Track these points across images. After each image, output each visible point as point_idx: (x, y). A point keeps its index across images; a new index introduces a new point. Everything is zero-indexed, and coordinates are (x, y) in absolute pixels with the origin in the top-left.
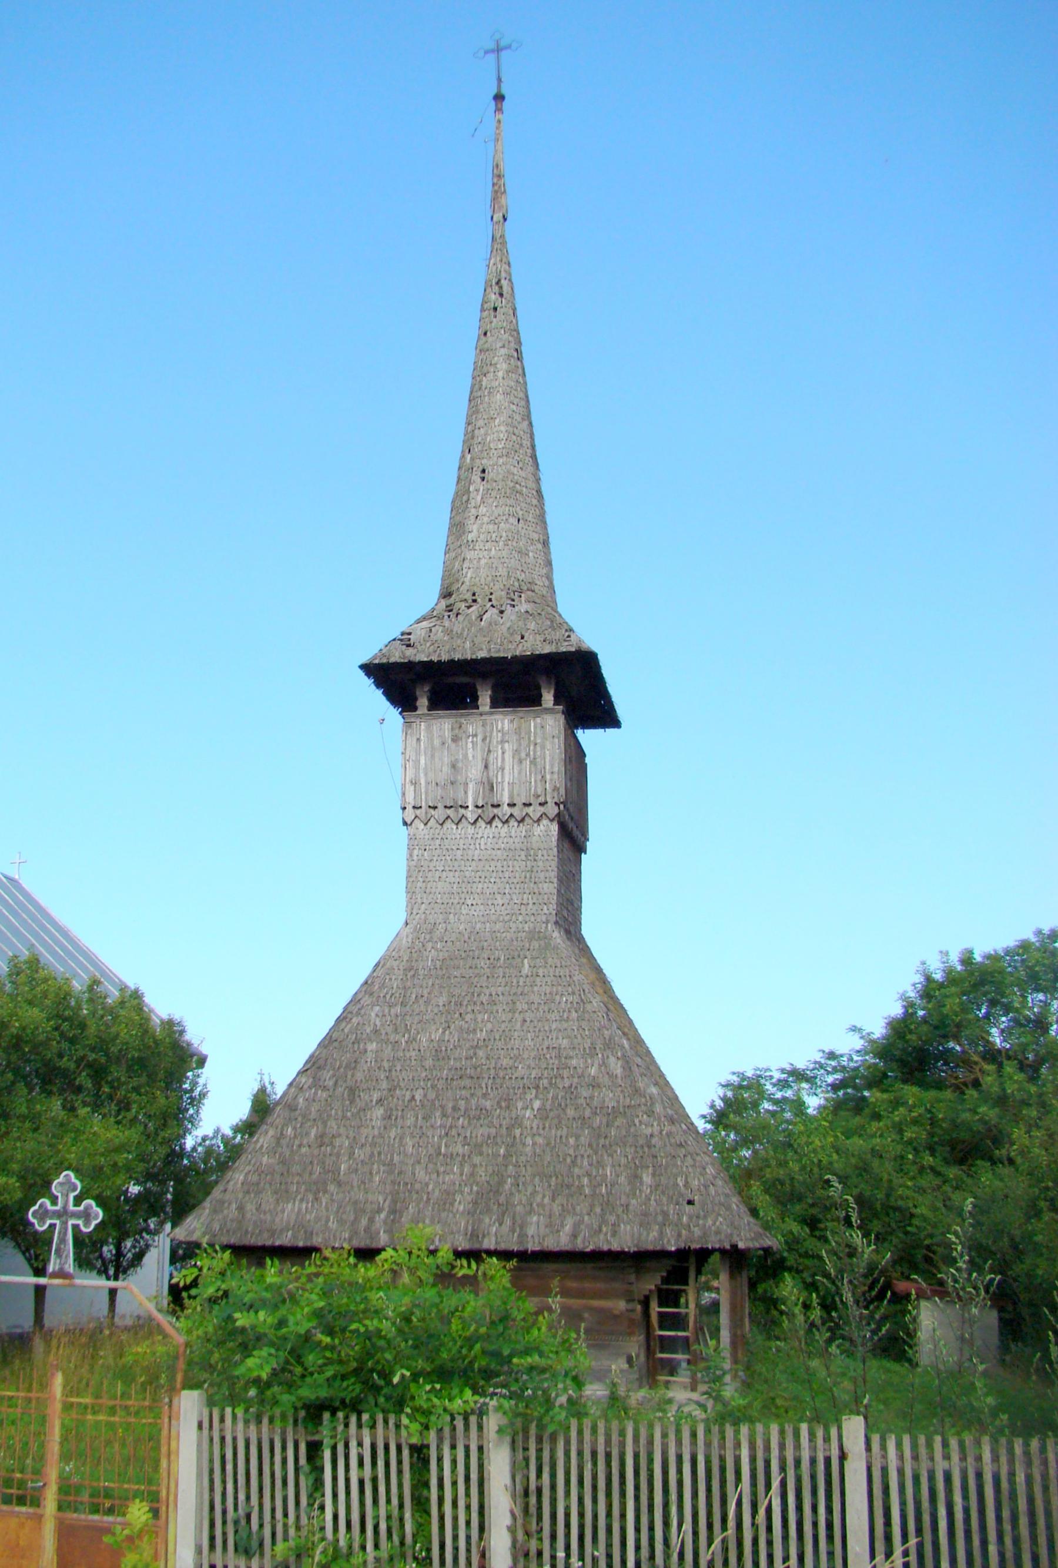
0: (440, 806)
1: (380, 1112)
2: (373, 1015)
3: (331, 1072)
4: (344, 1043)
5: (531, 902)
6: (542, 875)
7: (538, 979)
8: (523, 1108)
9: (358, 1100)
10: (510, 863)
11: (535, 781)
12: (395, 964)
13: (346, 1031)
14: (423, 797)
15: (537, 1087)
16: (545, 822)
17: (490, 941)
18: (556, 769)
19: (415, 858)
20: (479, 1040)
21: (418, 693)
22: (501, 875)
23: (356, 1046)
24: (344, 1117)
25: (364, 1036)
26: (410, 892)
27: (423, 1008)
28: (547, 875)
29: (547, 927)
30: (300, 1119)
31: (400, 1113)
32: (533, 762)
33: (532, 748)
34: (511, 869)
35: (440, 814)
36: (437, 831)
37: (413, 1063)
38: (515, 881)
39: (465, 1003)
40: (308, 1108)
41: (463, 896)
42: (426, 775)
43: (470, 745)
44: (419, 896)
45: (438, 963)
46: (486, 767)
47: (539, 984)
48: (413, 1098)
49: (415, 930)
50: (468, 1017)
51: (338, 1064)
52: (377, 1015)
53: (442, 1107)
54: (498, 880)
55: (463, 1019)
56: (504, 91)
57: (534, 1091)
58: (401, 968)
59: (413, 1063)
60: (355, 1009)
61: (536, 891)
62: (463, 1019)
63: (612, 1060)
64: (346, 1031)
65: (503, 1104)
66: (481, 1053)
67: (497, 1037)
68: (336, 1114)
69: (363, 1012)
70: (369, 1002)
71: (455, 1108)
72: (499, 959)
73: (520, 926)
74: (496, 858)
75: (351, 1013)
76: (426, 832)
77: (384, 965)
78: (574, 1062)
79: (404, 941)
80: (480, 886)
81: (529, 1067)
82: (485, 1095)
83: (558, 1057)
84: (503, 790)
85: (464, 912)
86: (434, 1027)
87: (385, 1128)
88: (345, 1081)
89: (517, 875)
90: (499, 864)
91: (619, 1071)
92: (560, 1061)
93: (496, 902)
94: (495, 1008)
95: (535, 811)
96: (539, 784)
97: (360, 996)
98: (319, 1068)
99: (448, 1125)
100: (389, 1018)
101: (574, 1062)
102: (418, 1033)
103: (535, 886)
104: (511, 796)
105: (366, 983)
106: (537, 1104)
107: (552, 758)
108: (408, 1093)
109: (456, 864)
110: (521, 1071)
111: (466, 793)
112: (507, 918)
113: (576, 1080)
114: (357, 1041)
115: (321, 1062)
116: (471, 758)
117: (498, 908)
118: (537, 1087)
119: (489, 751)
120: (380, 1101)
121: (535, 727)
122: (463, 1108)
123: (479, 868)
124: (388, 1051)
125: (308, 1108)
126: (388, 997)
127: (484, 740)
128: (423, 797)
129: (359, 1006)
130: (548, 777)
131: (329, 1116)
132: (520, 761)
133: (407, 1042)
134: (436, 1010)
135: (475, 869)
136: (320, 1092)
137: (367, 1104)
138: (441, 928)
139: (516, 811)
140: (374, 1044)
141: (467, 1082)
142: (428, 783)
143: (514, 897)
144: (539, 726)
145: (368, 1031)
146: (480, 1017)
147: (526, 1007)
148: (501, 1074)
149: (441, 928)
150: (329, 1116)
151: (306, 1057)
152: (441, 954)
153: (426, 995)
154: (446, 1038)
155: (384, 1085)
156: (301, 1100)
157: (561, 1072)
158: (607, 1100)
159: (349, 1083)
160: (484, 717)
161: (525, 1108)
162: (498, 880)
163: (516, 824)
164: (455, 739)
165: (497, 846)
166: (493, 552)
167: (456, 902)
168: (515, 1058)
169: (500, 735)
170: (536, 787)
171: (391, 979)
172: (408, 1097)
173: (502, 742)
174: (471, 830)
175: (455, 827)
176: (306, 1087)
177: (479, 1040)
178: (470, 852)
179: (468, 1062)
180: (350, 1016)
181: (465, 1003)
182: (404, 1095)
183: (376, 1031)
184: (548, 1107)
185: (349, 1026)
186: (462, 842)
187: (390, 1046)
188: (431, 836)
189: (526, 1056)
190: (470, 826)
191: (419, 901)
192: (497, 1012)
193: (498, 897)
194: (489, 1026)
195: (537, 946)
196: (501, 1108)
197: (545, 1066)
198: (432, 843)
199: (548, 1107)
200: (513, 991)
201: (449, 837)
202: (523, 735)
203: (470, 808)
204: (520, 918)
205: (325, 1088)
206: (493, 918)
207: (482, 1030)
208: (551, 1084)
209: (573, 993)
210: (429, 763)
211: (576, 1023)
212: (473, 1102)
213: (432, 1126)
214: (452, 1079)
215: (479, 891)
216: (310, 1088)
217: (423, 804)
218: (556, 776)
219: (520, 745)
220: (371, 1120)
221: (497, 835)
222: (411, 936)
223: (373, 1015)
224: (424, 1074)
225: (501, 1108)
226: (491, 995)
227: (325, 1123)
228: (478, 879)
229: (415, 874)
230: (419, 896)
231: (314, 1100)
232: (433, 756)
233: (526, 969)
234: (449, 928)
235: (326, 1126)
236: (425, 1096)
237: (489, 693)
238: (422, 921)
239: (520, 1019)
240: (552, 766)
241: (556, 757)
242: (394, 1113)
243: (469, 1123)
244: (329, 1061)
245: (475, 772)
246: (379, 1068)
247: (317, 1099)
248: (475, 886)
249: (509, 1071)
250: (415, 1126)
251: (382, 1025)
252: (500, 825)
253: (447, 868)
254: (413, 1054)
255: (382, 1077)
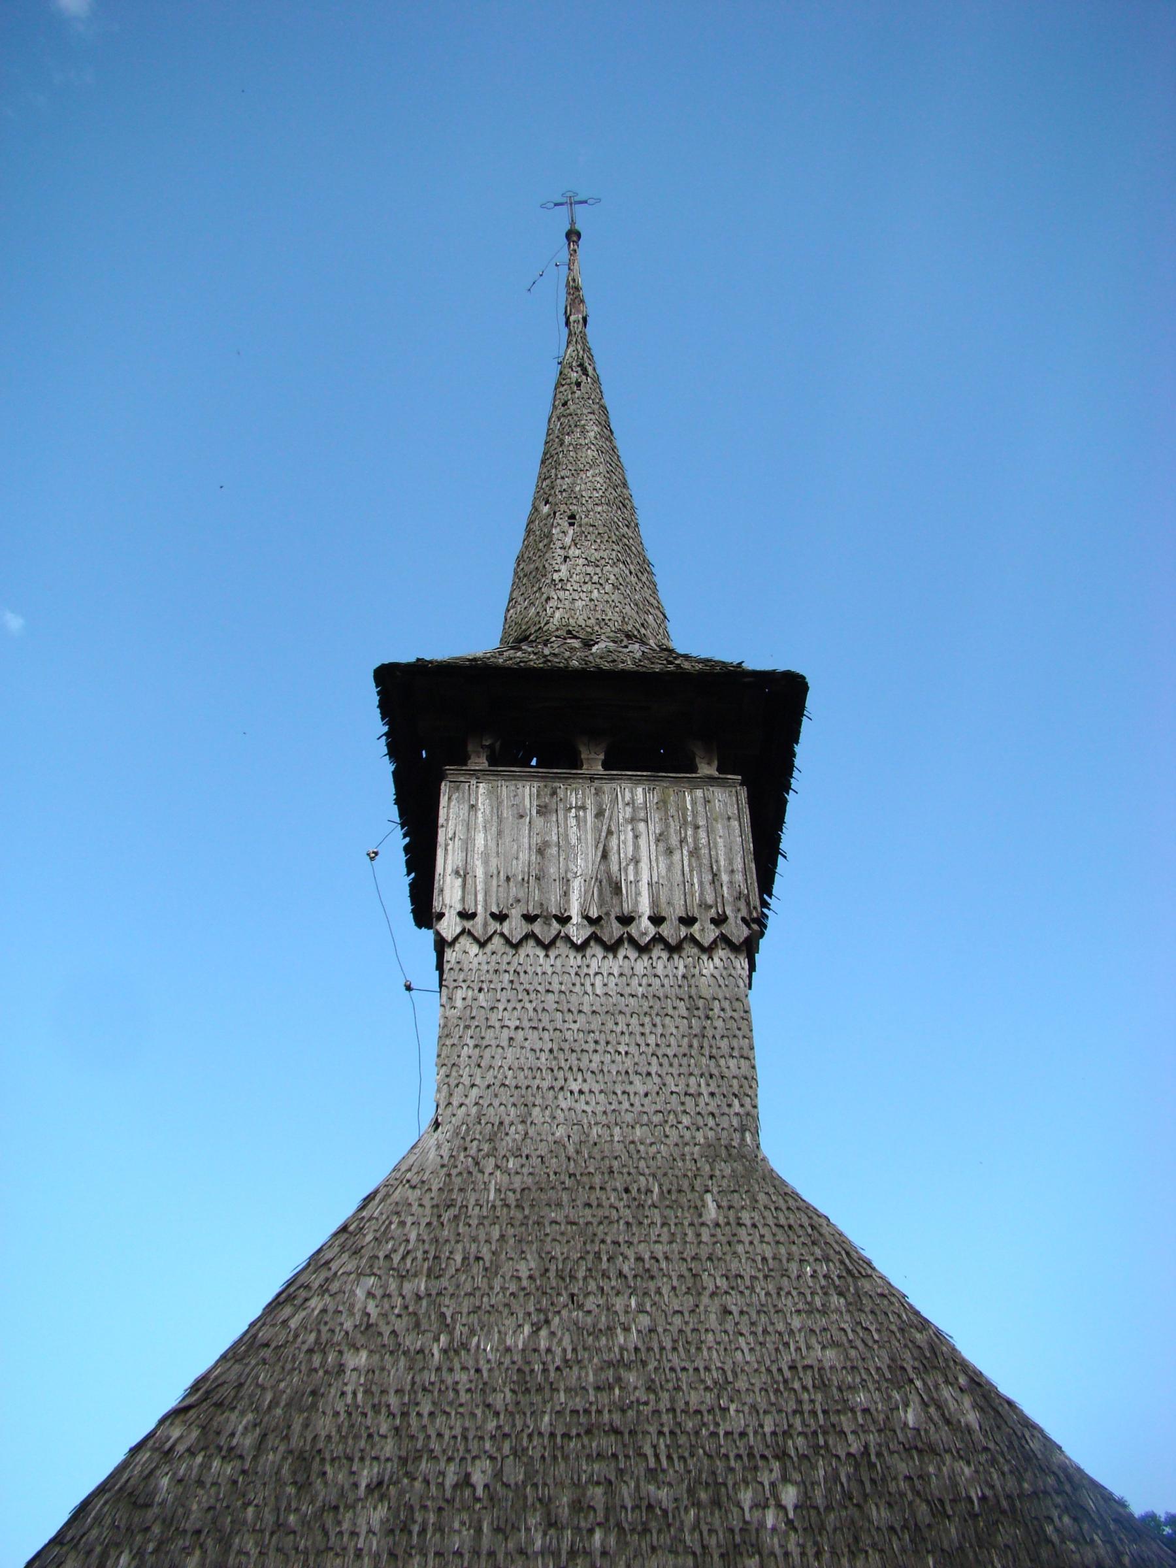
0: (516, 913)
1: (377, 1515)
2: (360, 1293)
3: (250, 1416)
4: (288, 1351)
5: (704, 1090)
6: (724, 1044)
7: (742, 1233)
8: (755, 1506)
9: (318, 1484)
10: (658, 1020)
11: (701, 884)
12: (413, 1195)
13: (293, 1324)
14: (480, 897)
15: (782, 1455)
16: (721, 953)
17: (625, 1156)
18: (738, 865)
19: (459, 1003)
20: (622, 1349)
21: (470, 748)
22: (640, 1040)
23: (317, 1360)
24: (279, 1526)
25: (338, 1337)
26: (447, 1064)
27: (480, 1281)
28: (735, 1043)
29: (743, 1139)
30: (156, 1529)
31: (432, 1518)
32: (694, 853)
33: (690, 832)
34: (659, 1030)
35: (515, 927)
36: (506, 959)
37: (464, 1397)
38: (670, 1052)
39: (581, 1274)
40: (181, 1501)
41: (561, 1075)
42: (486, 863)
43: (573, 822)
44: (466, 1073)
45: (511, 1198)
46: (605, 856)
47: (747, 1239)
48: (466, 1481)
49: (457, 1133)
50: (590, 1303)
51: (269, 1396)
52: (370, 1294)
53: (546, 1503)
54: (633, 1049)
55: (580, 1307)
56: (578, 227)
57: (776, 1465)
58: (427, 1202)
59: (464, 1397)
60: (316, 1281)
61: (715, 1071)
62: (580, 1307)
63: (947, 1393)
64: (293, 1324)
65: (703, 1496)
66: (631, 1378)
67: (668, 1344)
68: (258, 1516)
69: (335, 1286)
70: (350, 1267)
71: (578, 1506)
72: (649, 1191)
73: (687, 1134)
74: (627, 1011)
75: (307, 1287)
76: (481, 958)
77: (388, 1195)
78: (861, 1398)
79: (432, 1155)
80: (596, 1058)
81: (754, 1408)
82: (652, 1474)
83: (822, 1385)
84: (638, 894)
85: (564, 1105)
86: (510, 1322)
87: (392, 1555)
88: (287, 1438)
89: (672, 1040)
90: (634, 1021)
91: (972, 1418)
92: (826, 1396)
93: (629, 1088)
94: (652, 1285)
95: (707, 933)
96: (709, 889)
97: (329, 1255)
98: (219, 1405)
99: (565, 1547)
100: (399, 1301)
101: (861, 1398)
102: (472, 1332)
103: (712, 1063)
104: (654, 903)
105: (344, 1229)
106: (790, 1495)
107: (730, 849)
108: (452, 1468)
109: (545, 1017)
110: (736, 1420)
111: (566, 894)
112: (657, 1119)
113: (872, 1439)
114: (320, 1347)
115: (226, 1392)
116: (574, 841)
117: (636, 1101)
118: (782, 1455)
119: (610, 833)
120: (377, 1488)
121: (694, 803)
122: (600, 1507)
123: (593, 1027)
124: (397, 1373)
125: (181, 1501)
126: (396, 1258)
127: (599, 814)
128: (480, 897)
129: (324, 1274)
130: (725, 878)
131: (239, 1525)
132: (669, 852)
133: (445, 1351)
134: (513, 1287)
135: (587, 1027)
136: (216, 1463)
137: (342, 1495)
138: (515, 1133)
139: (666, 930)
140: (364, 1354)
141: (608, 1444)
142: (489, 876)
143: (669, 1080)
144: (700, 801)
145: (348, 1325)
146: (619, 1303)
147: (722, 1283)
148: (689, 1425)
149: (515, 1133)
150: (239, 1525)
151: (189, 1381)
152: (517, 1180)
153: (487, 1257)
154: (543, 1344)
155: (389, 1448)
156: (165, 1481)
157: (834, 1419)
158: (962, 1481)
159: (295, 1442)
160: (596, 784)
161: (763, 1506)
162: (633, 1049)
163: (665, 955)
164: (543, 810)
165: (627, 991)
166: (595, 594)
167: (545, 1085)
168: (721, 1386)
169: (629, 809)
170: (702, 894)
171: (402, 1224)
172: (451, 1477)
173: (633, 820)
174: (574, 959)
175: (542, 954)
176: (181, 1448)
177: (622, 1349)
178: (574, 999)
179: (604, 1398)
180: (303, 1294)
181: (581, 1274)
182: (442, 1474)
183: (368, 1327)
184: (820, 1501)
185: (302, 1314)
186: (555, 979)
187: (402, 1362)
188: (491, 968)
189: (742, 1384)
190: (572, 954)
191: (466, 1080)
192: (659, 1292)
193: (637, 1080)
194: (644, 1321)
195: (728, 1172)
196: (698, 1504)
197: (792, 1405)
198: (495, 978)
199: (820, 1501)
200: (689, 1252)
201: (530, 970)
202: (672, 811)
203: (574, 921)
204: (686, 1120)
205: (231, 1454)
206: (629, 1118)
207: (627, 1329)
208: (816, 1448)
209: (827, 1259)
210: (492, 844)
211: (847, 1317)
212: (626, 1492)
213: (522, 1552)
214: (566, 1436)
215: (594, 1066)
216: (191, 1452)
217: (480, 909)
218: (739, 877)
219: (667, 826)
220: (354, 1534)
221: (627, 971)
222: (446, 1146)
223: (360, 1293)
224: (491, 1425)
225: (698, 1504)
226: (639, 1259)
227: (225, 1543)
228: (592, 1046)
229: (457, 1033)
230: (466, 1073)
231: (200, 1483)
232: (500, 833)
233: (711, 1212)
234: (531, 1132)
235: (226, 1551)
236: (498, 1475)
237: (602, 757)
238: (470, 1120)
239: (715, 1307)
240: (731, 861)
241: (737, 848)
242: (418, 1517)
243: (622, 1543)
244: (246, 1391)
245: (584, 863)
246: (376, 1408)
247: (208, 1481)
248: (585, 1057)
249: (708, 1418)
250: (476, 1553)
251: (384, 1315)
252: (633, 954)
253: (526, 1024)
254: (463, 1377)
255: (384, 1429)
